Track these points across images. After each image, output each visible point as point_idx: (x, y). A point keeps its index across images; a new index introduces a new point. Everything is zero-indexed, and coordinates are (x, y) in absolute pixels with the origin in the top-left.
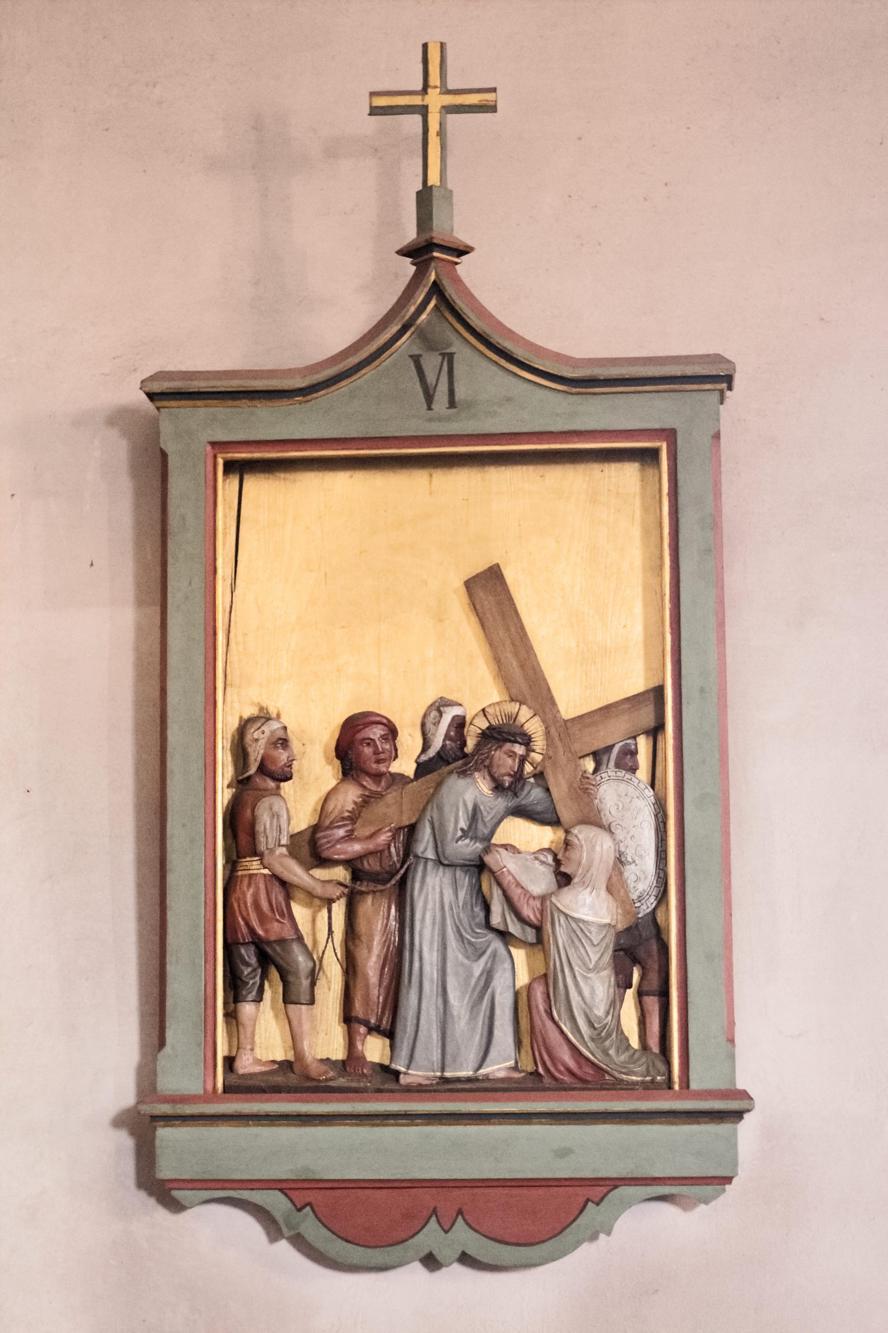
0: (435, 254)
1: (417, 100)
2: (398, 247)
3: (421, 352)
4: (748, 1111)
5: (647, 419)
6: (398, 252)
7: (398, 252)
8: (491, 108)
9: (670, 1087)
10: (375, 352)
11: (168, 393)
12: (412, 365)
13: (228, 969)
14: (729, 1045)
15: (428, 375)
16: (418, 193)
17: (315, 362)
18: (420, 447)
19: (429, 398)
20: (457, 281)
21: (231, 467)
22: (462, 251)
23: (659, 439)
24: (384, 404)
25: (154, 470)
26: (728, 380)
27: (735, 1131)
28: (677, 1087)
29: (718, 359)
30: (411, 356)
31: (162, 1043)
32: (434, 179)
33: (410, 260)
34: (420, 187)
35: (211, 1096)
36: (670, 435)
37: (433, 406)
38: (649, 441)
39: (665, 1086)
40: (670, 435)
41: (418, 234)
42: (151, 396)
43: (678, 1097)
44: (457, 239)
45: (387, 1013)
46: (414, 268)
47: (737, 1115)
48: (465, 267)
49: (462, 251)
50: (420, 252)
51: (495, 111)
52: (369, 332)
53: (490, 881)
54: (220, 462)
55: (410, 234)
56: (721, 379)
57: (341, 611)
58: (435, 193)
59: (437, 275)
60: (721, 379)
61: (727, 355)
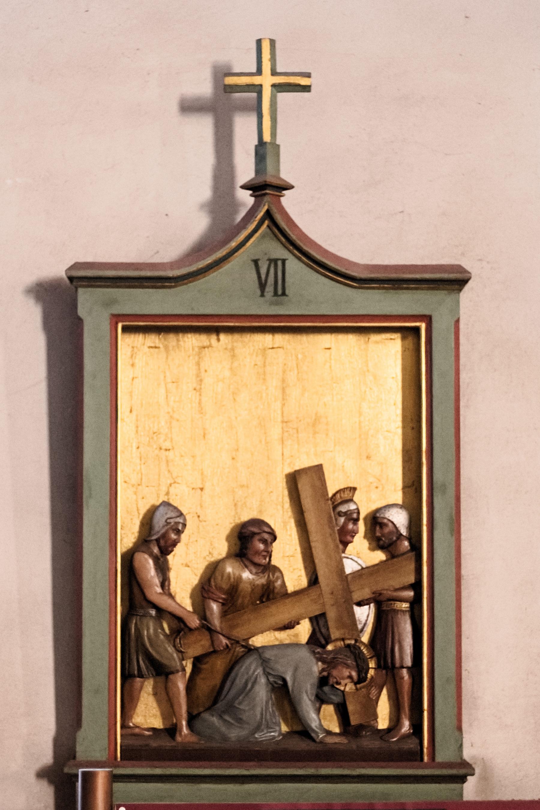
0: (268, 191)
5: (414, 304)
8: (306, 89)
9: (422, 759)
10: (225, 256)
11: (85, 278)
12: (253, 266)
13: (322, 478)
14: (457, 733)
15: (258, 268)
16: (256, 146)
17: (462, 590)
19: (262, 286)
21: (125, 329)
22: (289, 187)
23: (421, 321)
27: (462, 787)
28: (426, 758)
29: (459, 269)
32: (267, 138)
33: (250, 192)
34: (256, 143)
36: (428, 319)
37: (265, 294)
41: (256, 175)
43: (426, 766)
47: (462, 779)
48: (288, 200)
49: (289, 187)
51: (309, 91)
53: (293, 690)
54: (120, 326)
57: (222, 439)
59: (269, 206)
60: (454, 281)
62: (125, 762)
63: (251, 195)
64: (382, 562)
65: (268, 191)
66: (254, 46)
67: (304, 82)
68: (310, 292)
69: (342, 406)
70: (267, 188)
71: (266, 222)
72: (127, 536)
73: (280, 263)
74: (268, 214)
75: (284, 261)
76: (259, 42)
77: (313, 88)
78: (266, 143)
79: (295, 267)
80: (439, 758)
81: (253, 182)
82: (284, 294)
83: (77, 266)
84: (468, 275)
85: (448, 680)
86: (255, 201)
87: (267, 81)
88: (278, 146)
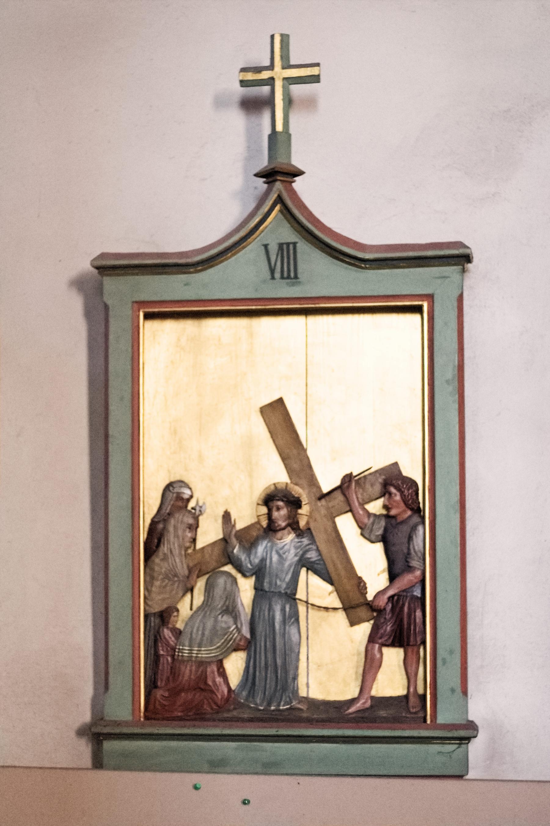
0: (279, 178)
1: (265, 75)
2: (255, 172)
3: (296, 240)
4: (475, 737)
5: (420, 276)
6: (256, 175)
7: (256, 175)
11: (110, 267)
15: (290, 256)
18: (188, 307)
20: (293, 194)
21: (148, 316)
22: (299, 173)
24: (244, 275)
25: (98, 316)
26: (467, 258)
28: (429, 722)
29: (460, 245)
30: (263, 245)
31: (107, 687)
32: (279, 127)
35: (136, 723)
36: (430, 298)
38: (409, 301)
39: (422, 720)
40: (430, 298)
42: (97, 268)
43: (428, 728)
44: (294, 166)
45: (406, 626)
46: (266, 186)
47: (468, 739)
48: (298, 184)
49: (299, 173)
50: (269, 175)
51: (318, 81)
52: (237, 227)
55: (263, 163)
56: (462, 258)
57: (214, 410)
58: (279, 137)
60: (462, 258)
61: (467, 244)
62: (148, 722)
63: (265, 183)
64: (417, 597)
65: (279, 178)
66: (269, 40)
67: (314, 71)
68: (320, 275)
69: (355, 390)
70: (278, 174)
71: (278, 208)
72: (150, 504)
73: (291, 247)
74: (280, 200)
75: (295, 244)
76: (318, 65)
77: (322, 77)
78: (277, 132)
79: (304, 248)
80: (441, 720)
81: (267, 169)
82: (296, 277)
83: (103, 256)
84: (467, 251)
85: (451, 652)
86: (268, 187)
87: (279, 73)
88: (290, 135)
